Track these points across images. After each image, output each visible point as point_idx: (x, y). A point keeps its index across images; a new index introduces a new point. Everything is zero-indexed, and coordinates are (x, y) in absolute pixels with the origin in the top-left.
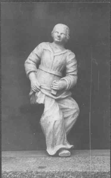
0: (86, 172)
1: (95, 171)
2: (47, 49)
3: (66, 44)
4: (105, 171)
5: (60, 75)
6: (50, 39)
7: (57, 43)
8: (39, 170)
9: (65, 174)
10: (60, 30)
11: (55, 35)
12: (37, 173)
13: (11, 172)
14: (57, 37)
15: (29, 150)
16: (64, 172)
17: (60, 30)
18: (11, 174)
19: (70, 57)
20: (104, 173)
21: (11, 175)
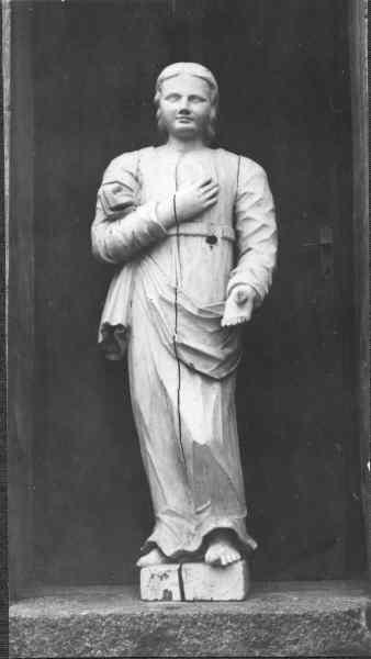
0: (259, 615)
1: (277, 613)
2: (127, 174)
3: (219, 132)
4: (297, 612)
5: (110, 254)
6: (149, 132)
7: (187, 138)
8: (167, 613)
9: (218, 619)
10: (183, 85)
11: (168, 107)
12: (164, 617)
13: (110, 615)
14: (180, 116)
15: (335, 578)
16: (216, 615)
17: (183, 85)
18: (109, 619)
19: (247, 178)
20: (296, 616)
21: (109, 622)
